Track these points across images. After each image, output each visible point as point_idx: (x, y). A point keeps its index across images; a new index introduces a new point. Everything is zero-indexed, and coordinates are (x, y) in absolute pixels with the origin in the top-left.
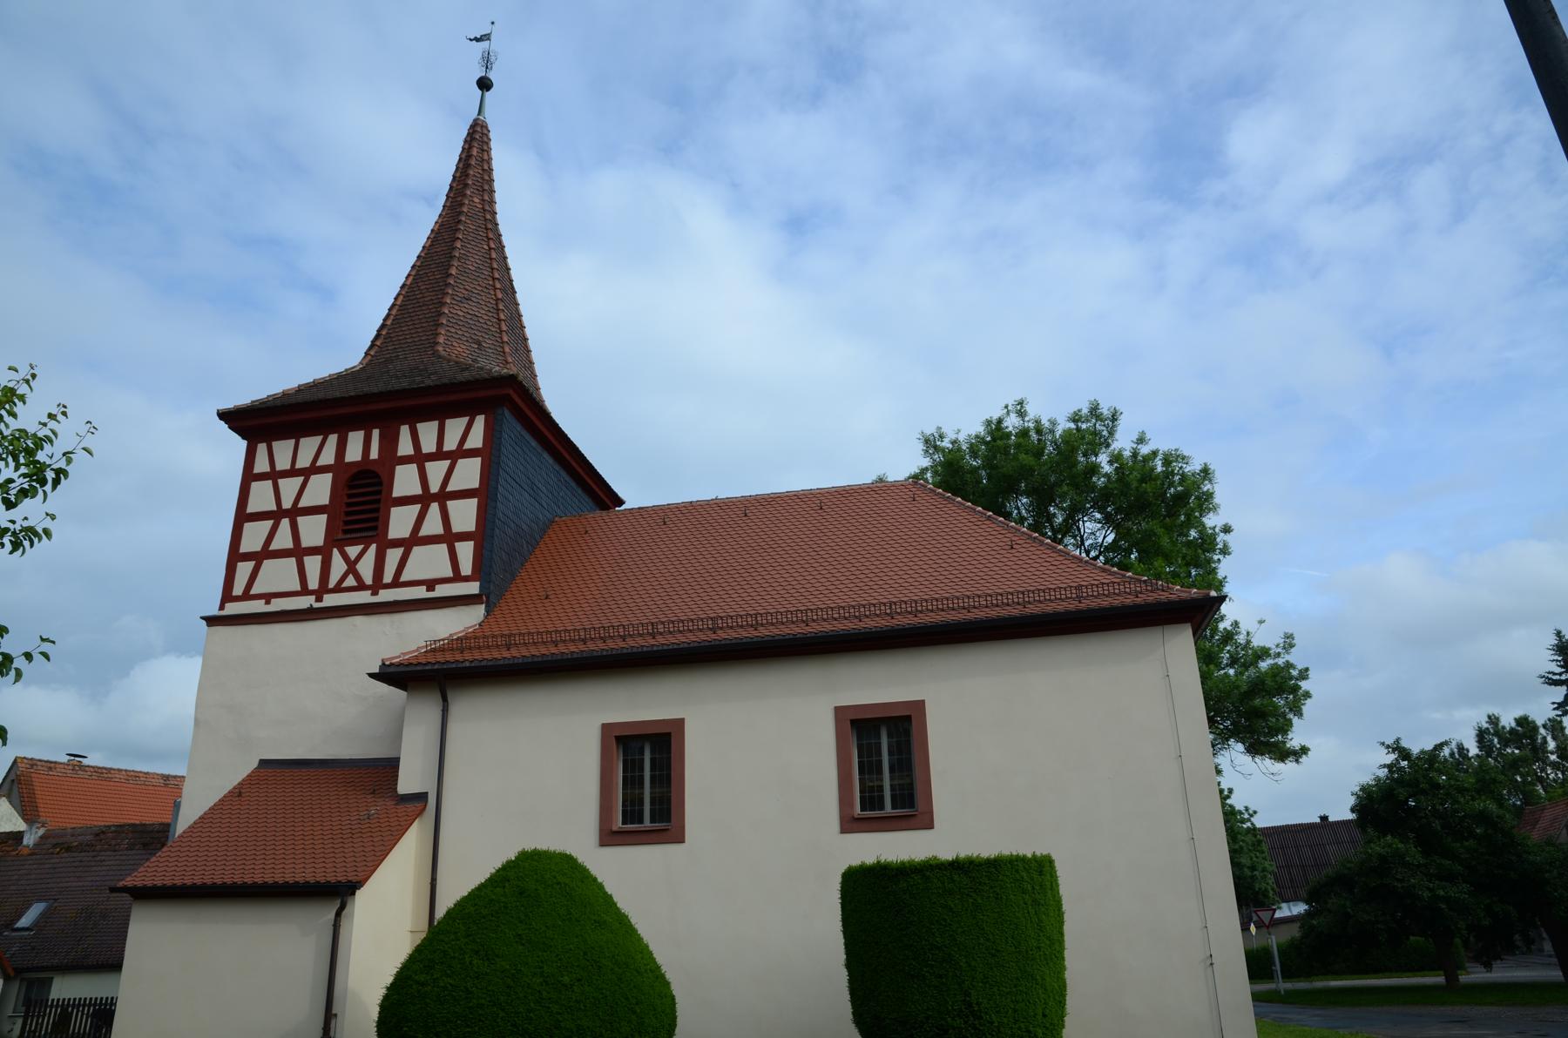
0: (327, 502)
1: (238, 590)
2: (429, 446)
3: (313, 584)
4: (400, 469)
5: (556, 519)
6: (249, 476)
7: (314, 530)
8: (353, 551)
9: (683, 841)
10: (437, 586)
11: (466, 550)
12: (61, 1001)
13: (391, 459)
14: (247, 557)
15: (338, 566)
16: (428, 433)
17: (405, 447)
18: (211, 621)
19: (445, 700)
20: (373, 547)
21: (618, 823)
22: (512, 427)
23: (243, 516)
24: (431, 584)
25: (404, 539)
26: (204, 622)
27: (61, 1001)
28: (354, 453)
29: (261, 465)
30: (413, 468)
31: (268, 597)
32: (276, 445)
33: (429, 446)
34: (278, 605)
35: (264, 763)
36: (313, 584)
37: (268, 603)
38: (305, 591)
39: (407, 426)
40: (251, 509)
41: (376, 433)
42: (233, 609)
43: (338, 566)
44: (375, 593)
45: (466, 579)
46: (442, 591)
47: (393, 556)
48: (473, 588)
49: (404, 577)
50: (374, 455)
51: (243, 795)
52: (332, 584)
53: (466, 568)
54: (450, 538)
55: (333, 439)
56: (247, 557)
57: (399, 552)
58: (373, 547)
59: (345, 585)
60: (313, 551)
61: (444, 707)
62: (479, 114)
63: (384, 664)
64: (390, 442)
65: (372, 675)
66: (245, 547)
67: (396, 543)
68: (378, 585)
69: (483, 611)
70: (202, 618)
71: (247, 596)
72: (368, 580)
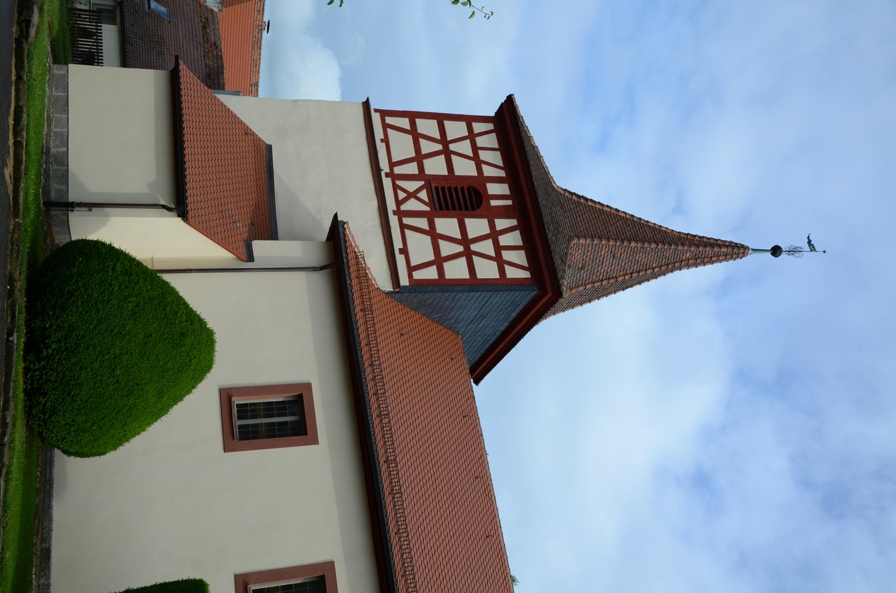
1: (389, 120)
2: (504, 240)
3: (398, 170)
4: (485, 221)
6: (469, 120)
7: (436, 167)
8: (423, 195)
11: (431, 273)
13: (492, 215)
14: (413, 124)
15: (412, 186)
16: (513, 238)
17: (501, 224)
18: (366, 105)
21: (237, 401)
22: (524, 297)
23: (441, 118)
24: (404, 251)
28: (493, 189)
29: (478, 127)
31: (386, 140)
32: (517, 233)
33: (504, 240)
34: (381, 148)
35: (269, 148)
36: (398, 170)
37: (382, 141)
38: (392, 165)
39: (517, 224)
40: (447, 123)
41: (509, 202)
42: (376, 118)
44: (395, 213)
45: (410, 276)
46: (400, 259)
47: (423, 223)
48: (404, 281)
50: (494, 203)
51: (246, 136)
52: (398, 182)
53: (418, 275)
54: (439, 261)
55: (502, 173)
56: (413, 124)
59: (399, 192)
60: (421, 168)
62: (752, 249)
63: (344, 223)
64: (504, 213)
65: (336, 216)
66: (419, 122)
67: (432, 224)
68: (400, 214)
70: (368, 99)
71: (385, 126)
72: (404, 207)
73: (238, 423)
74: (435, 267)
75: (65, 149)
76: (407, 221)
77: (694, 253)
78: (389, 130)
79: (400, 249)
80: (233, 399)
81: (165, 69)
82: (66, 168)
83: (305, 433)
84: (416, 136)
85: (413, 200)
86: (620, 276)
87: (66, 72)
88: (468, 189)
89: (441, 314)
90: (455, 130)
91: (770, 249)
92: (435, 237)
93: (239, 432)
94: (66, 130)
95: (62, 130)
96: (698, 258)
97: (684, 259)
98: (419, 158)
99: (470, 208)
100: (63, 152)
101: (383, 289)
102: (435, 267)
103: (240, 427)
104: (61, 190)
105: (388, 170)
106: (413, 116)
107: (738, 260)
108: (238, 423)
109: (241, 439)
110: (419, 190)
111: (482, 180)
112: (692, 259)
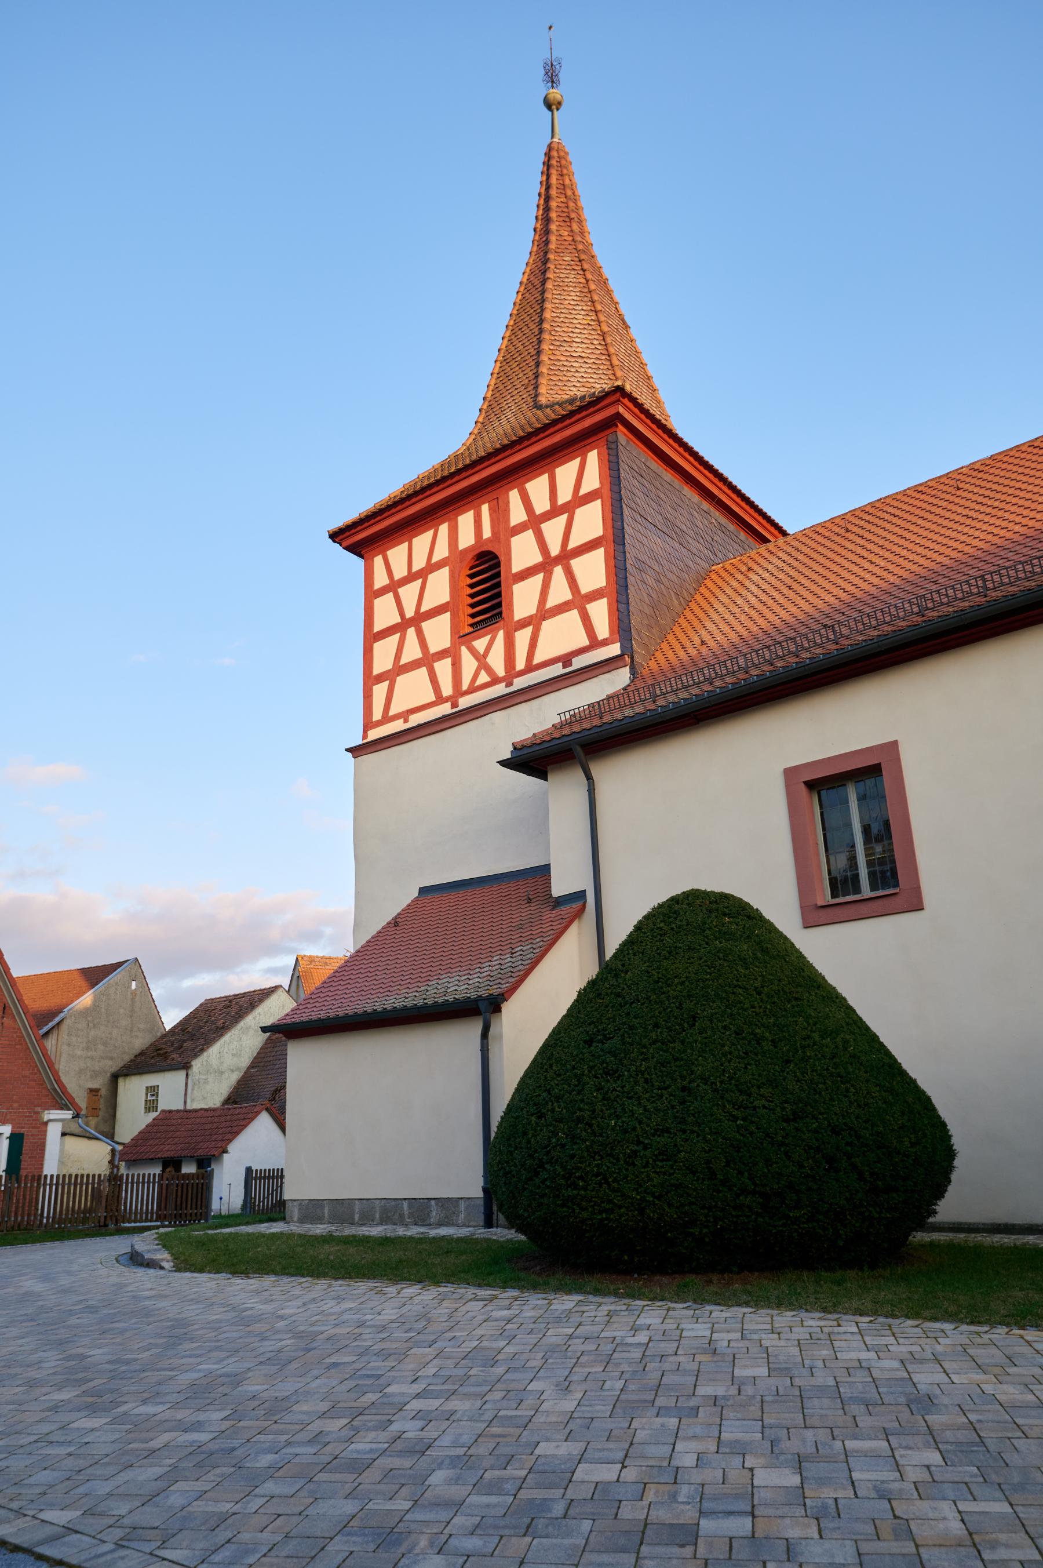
0: (447, 599)
1: (377, 715)
2: (542, 505)
3: (447, 690)
4: (515, 541)
5: (713, 568)
6: (372, 594)
8: (480, 644)
9: (920, 908)
10: (573, 660)
11: (600, 612)
12: (97, 1177)
13: (504, 531)
14: (380, 678)
15: (469, 664)
16: (538, 488)
17: (517, 514)
18: (355, 751)
19: (589, 777)
20: (501, 634)
21: (825, 896)
22: (632, 453)
23: (372, 637)
24: (566, 659)
25: (531, 617)
26: (350, 755)
27: (97, 1177)
28: (466, 539)
29: (381, 580)
30: (585, 588)
31: (405, 715)
33: (542, 505)
34: (416, 720)
35: (423, 891)
36: (447, 690)
37: (406, 721)
38: (440, 700)
39: (516, 490)
40: (377, 627)
41: (485, 508)
42: (374, 734)
43: (469, 664)
45: (605, 643)
46: (578, 663)
47: (523, 638)
48: (615, 649)
49: (538, 659)
50: (487, 533)
51: (400, 924)
52: (465, 687)
53: (603, 630)
54: (580, 601)
55: (444, 529)
56: (380, 678)
57: (528, 631)
58: (501, 634)
59: (478, 682)
60: (442, 654)
61: (589, 785)
62: (553, 137)
63: (515, 748)
64: (500, 514)
65: (504, 763)
66: (377, 669)
67: (523, 624)
69: (629, 675)
70: (347, 750)
71: (386, 719)
72: (501, 672)
73: (866, 891)
74: (588, 607)
75: (405, 1204)
76: (520, 664)
77: (561, 224)
78: (391, 713)
79: (564, 667)
80: (820, 903)
81: (286, 1045)
82: (433, 1202)
83: (875, 770)
84: (400, 669)
85: (489, 660)
86: (604, 339)
87: (295, 1203)
88: (471, 576)
89: (672, 593)
90: (386, 614)
91: (550, 113)
92: (544, 613)
93: (883, 889)
94: (377, 1202)
95: (378, 1209)
96: (568, 217)
97: (571, 238)
98: (428, 660)
99: (496, 561)
100: (410, 1207)
101: (628, 682)
102: (588, 607)
103: (873, 888)
104: (466, 1208)
105: (449, 704)
106: (370, 680)
107: (570, 158)
108: (866, 891)
109: (896, 885)
110: (473, 652)
111: (454, 559)
112: (570, 226)
